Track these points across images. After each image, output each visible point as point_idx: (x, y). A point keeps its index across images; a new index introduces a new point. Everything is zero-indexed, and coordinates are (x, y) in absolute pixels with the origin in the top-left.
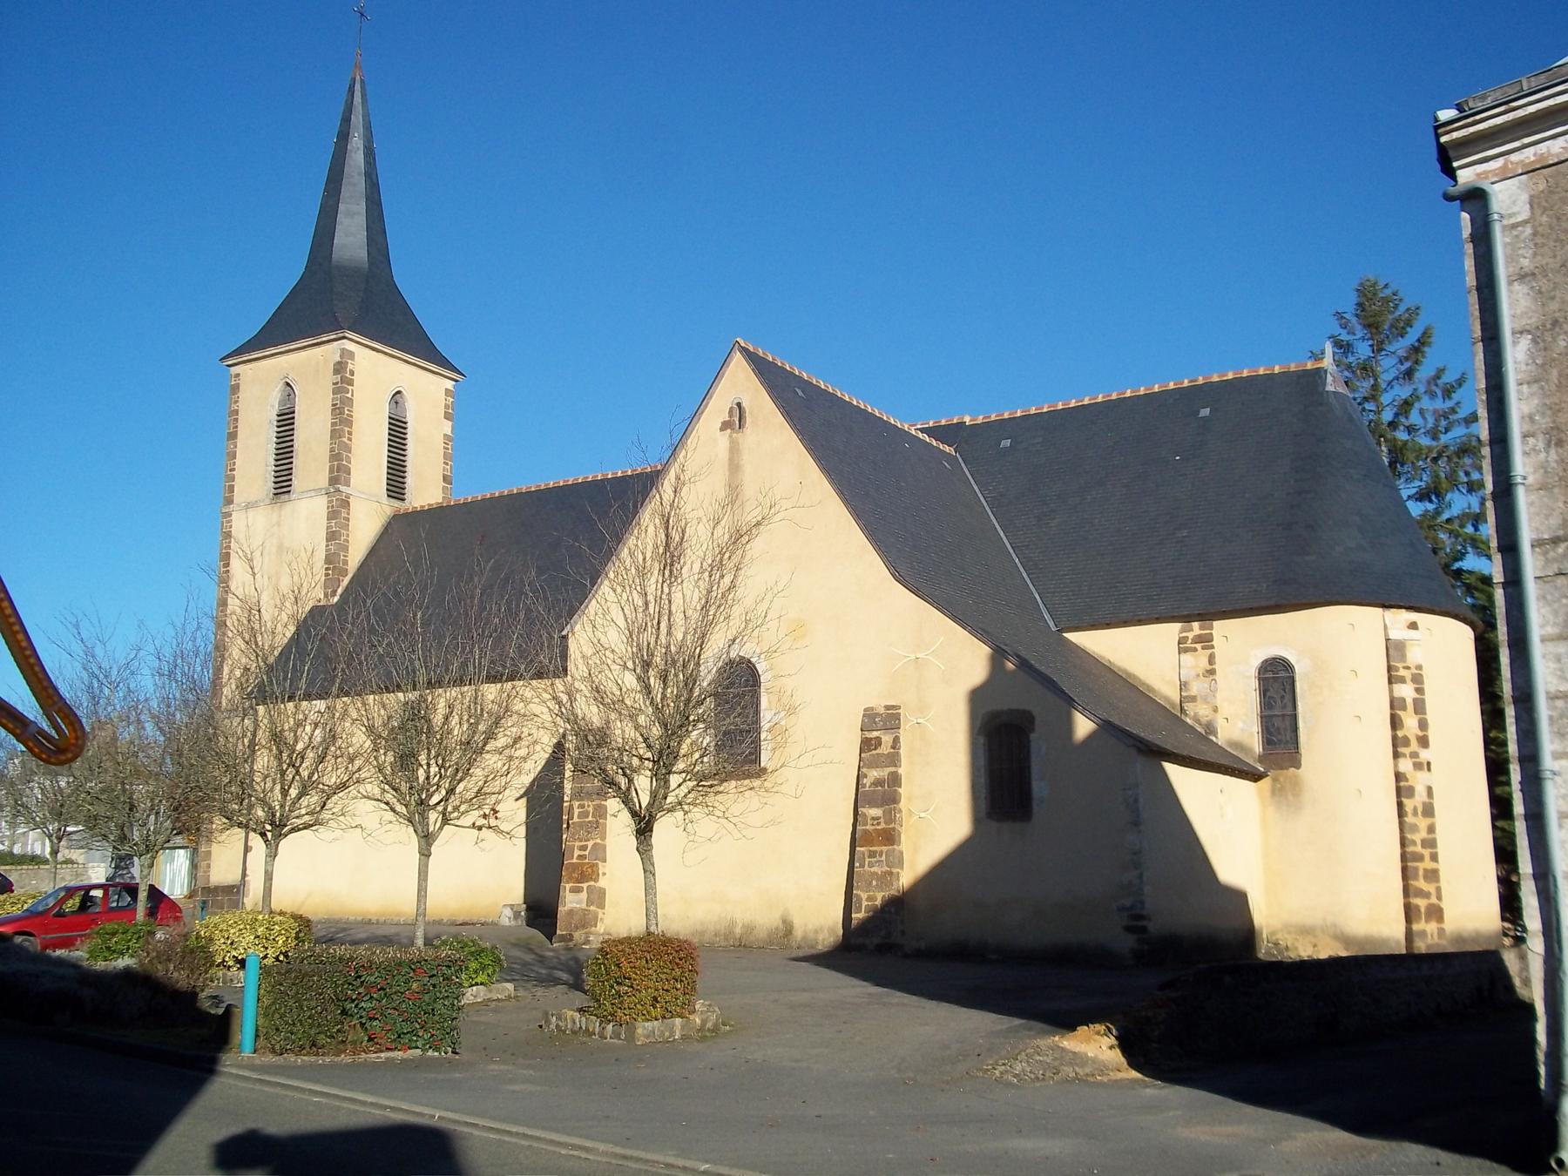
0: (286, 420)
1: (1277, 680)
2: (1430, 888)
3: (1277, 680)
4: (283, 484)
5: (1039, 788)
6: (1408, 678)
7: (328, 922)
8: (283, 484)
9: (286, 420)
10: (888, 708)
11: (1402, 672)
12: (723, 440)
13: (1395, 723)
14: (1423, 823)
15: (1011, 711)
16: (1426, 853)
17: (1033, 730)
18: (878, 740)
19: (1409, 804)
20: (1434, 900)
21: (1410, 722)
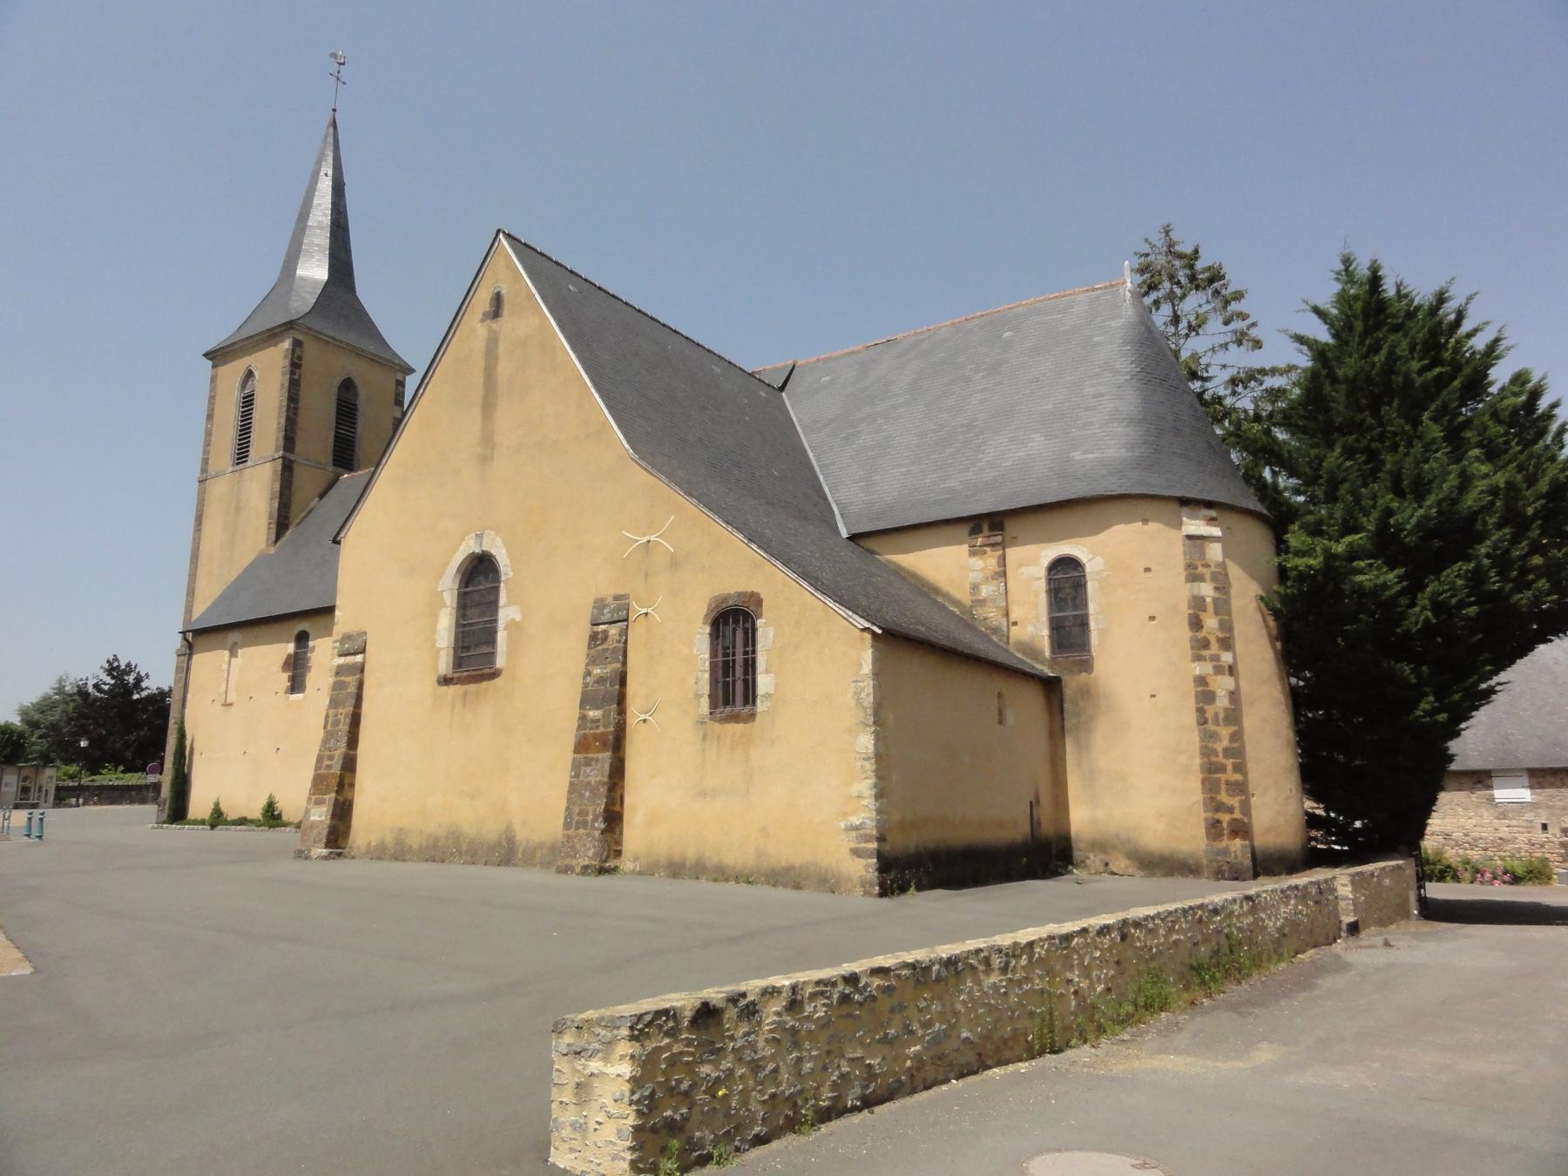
0: (248, 402)
1: (1066, 581)
2: (1234, 802)
3: (1066, 581)
4: (242, 455)
5: (764, 683)
6: (1208, 577)
7: (1154, 875)
8: (242, 455)
9: (248, 402)
10: (617, 598)
11: (1201, 570)
12: (482, 330)
13: (1196, 624)
14: (1225, 732)
15: (739, 594)
16: (1229, 763)
17: (760, 616)
18: (605, 632)
19: (1210, 711)
20: (1237, 815)
21: (1211, 622)
